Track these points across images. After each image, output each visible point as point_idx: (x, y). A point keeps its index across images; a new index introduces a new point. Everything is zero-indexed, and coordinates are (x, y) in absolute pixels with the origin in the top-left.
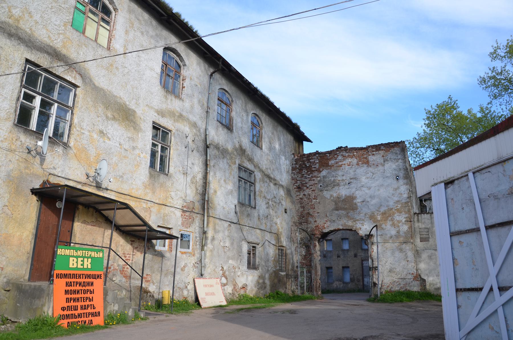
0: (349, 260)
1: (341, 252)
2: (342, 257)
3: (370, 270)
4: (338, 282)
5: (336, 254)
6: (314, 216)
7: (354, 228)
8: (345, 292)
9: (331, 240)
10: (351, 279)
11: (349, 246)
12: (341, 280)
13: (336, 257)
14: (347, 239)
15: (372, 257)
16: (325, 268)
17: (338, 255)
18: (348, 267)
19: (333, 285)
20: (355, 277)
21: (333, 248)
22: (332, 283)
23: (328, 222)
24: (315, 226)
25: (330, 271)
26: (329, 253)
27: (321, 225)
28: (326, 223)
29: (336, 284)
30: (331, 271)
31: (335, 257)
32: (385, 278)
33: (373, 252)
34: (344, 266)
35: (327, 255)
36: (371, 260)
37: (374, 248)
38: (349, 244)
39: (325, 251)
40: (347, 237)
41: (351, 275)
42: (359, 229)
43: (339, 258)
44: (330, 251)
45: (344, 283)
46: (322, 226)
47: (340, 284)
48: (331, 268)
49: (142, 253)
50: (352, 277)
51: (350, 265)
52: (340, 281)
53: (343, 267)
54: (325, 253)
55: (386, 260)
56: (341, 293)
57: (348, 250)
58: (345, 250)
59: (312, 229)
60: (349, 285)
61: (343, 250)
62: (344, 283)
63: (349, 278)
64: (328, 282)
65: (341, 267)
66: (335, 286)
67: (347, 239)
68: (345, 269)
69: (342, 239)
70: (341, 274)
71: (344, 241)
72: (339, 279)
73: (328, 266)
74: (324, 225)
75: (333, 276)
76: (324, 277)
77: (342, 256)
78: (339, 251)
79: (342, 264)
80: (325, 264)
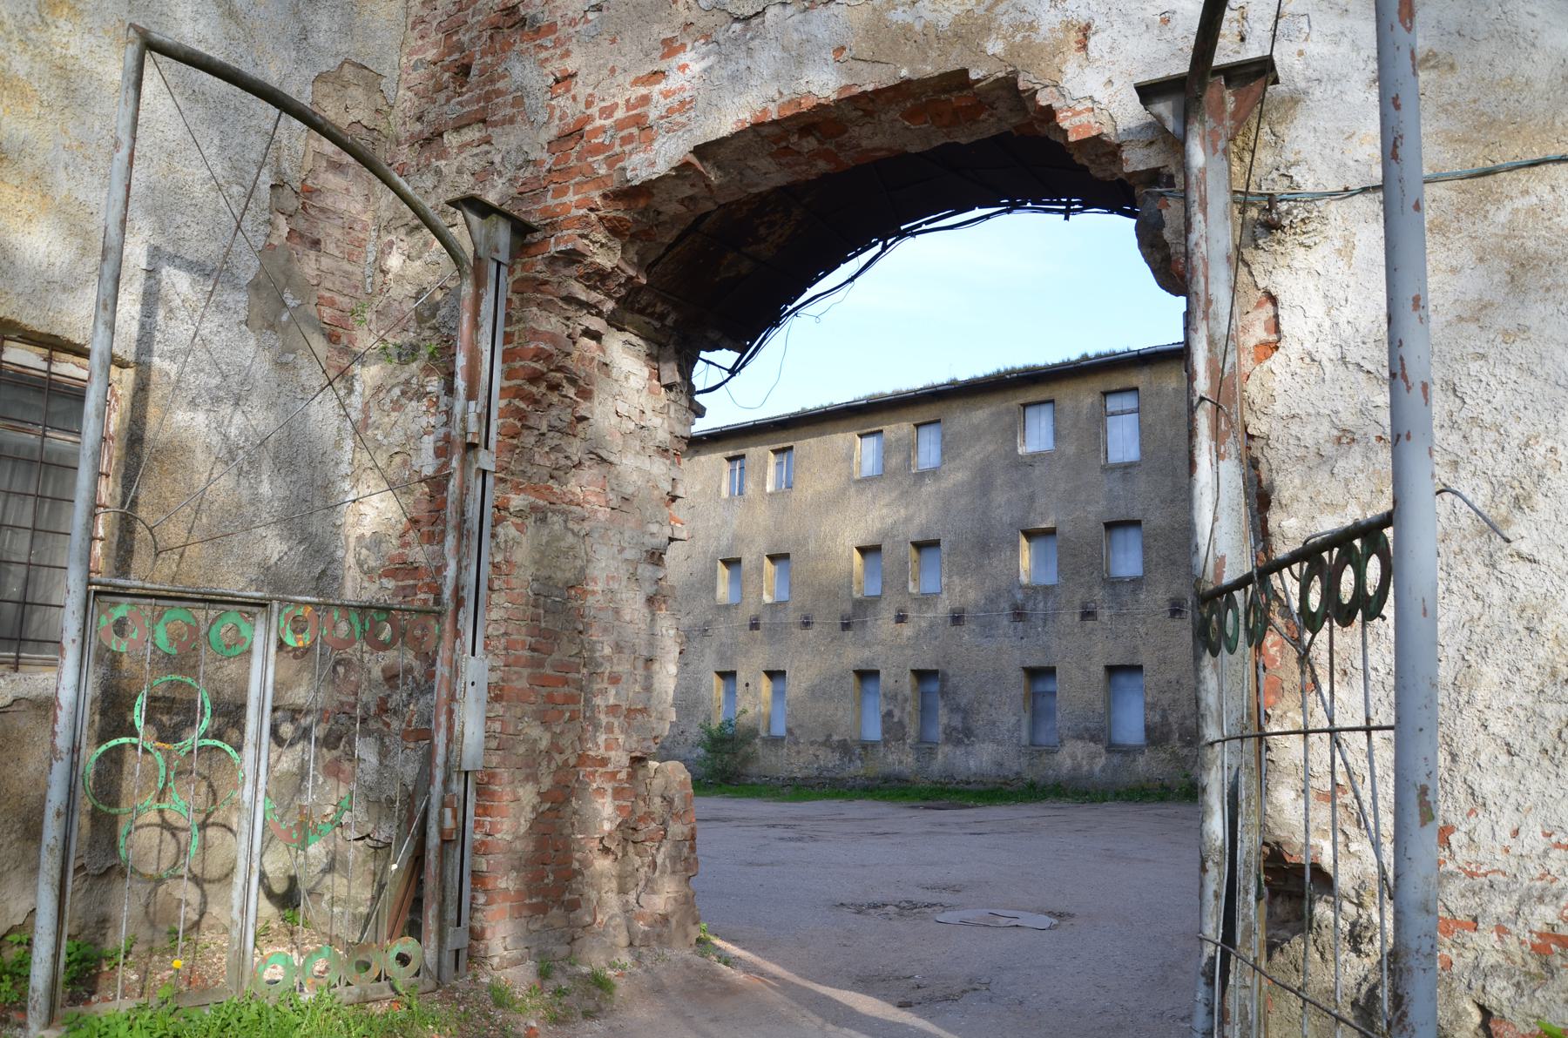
0: (1142, 630)
1: (1099, 594)
2: (1104, 614)
3: (1209, 640)
4: (1080, 744)
5: (1077, 602)
6: (552, 27)
7: (995, 47)
8: (1117, 796)
9: (1051, 532)
10: (1149, 729)
11: (1146, 564)
12: (1100, 734)
13: (1077, 618)
14: (1136, 523)
15: (1257, 426)
16: (1021, 674)
17: (1084, 606)
18: (1137, 669)
19: (1058, 757)
20: (1173, 718)
21: (1059, 573)
22: (1052, 750)
23: (685, 57)
24: (553, 131)
25: (1041, 686)
26: (1040, 598)
27: (607, 112)
28: (657, 75)
29: (1074, 757)
30: (1050, 687)
31: (1070, 618)
32: (1488, 785)
33: (1270, 348)
34: (1115, 661)
35: (1030, 605)
36: (1231, 472)
37: (1284, 284)
38: (1146, 549)
39: (1021, 587)
40: (1136, 515)
41: (1150, 707)
42: (1057, 50)
43: (1090, 624)
44: (1047, 590)
45: (1112, 748)
46: (620, 114)
47: (1093, 757)
48: (1048, 672)
49: (9, 571)
50: (1157, 718)
51: (1144, 658)
52: (1094, 739)
53: (1112, 670)
54: (1019, 596)
55: (1503, 466)
56: (1093, 801)
57: (1136, 582)
58: (1121, 581)
59: (527, 173)
60: (1141, 760)
61: (1113, 583)
62: (1112, 748)
63: (1141, 726)
64: (1032, 744)
65: (1098, 671)
66: (1068, 763)
67: (1136, 523)
68: (1122, 680)
69: (1111, 526)
70: (1099, 706)
71: (1119, 535)
72: (1087, 729)
73: (1033, 662)
74: (645, 100)
75: (1059, 715)
76: (1013, 720)
77: (1107, 612)
78: (1090, 588)
79: (1106, 651)
80: (1017, 653)
